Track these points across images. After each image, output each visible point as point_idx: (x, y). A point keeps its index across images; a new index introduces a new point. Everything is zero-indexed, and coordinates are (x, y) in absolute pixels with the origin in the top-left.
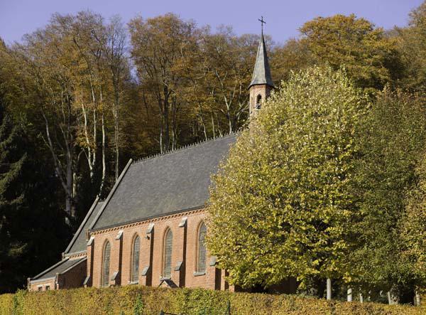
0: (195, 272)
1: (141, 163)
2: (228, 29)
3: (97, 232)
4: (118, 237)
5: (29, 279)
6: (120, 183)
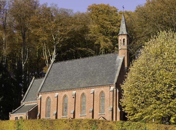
0: (62, 116)
1: (59, 64)
2: (56, 5)
3: (43, 93)
4: (56, 96)
5: (10, 113)
6: (49, 72)
